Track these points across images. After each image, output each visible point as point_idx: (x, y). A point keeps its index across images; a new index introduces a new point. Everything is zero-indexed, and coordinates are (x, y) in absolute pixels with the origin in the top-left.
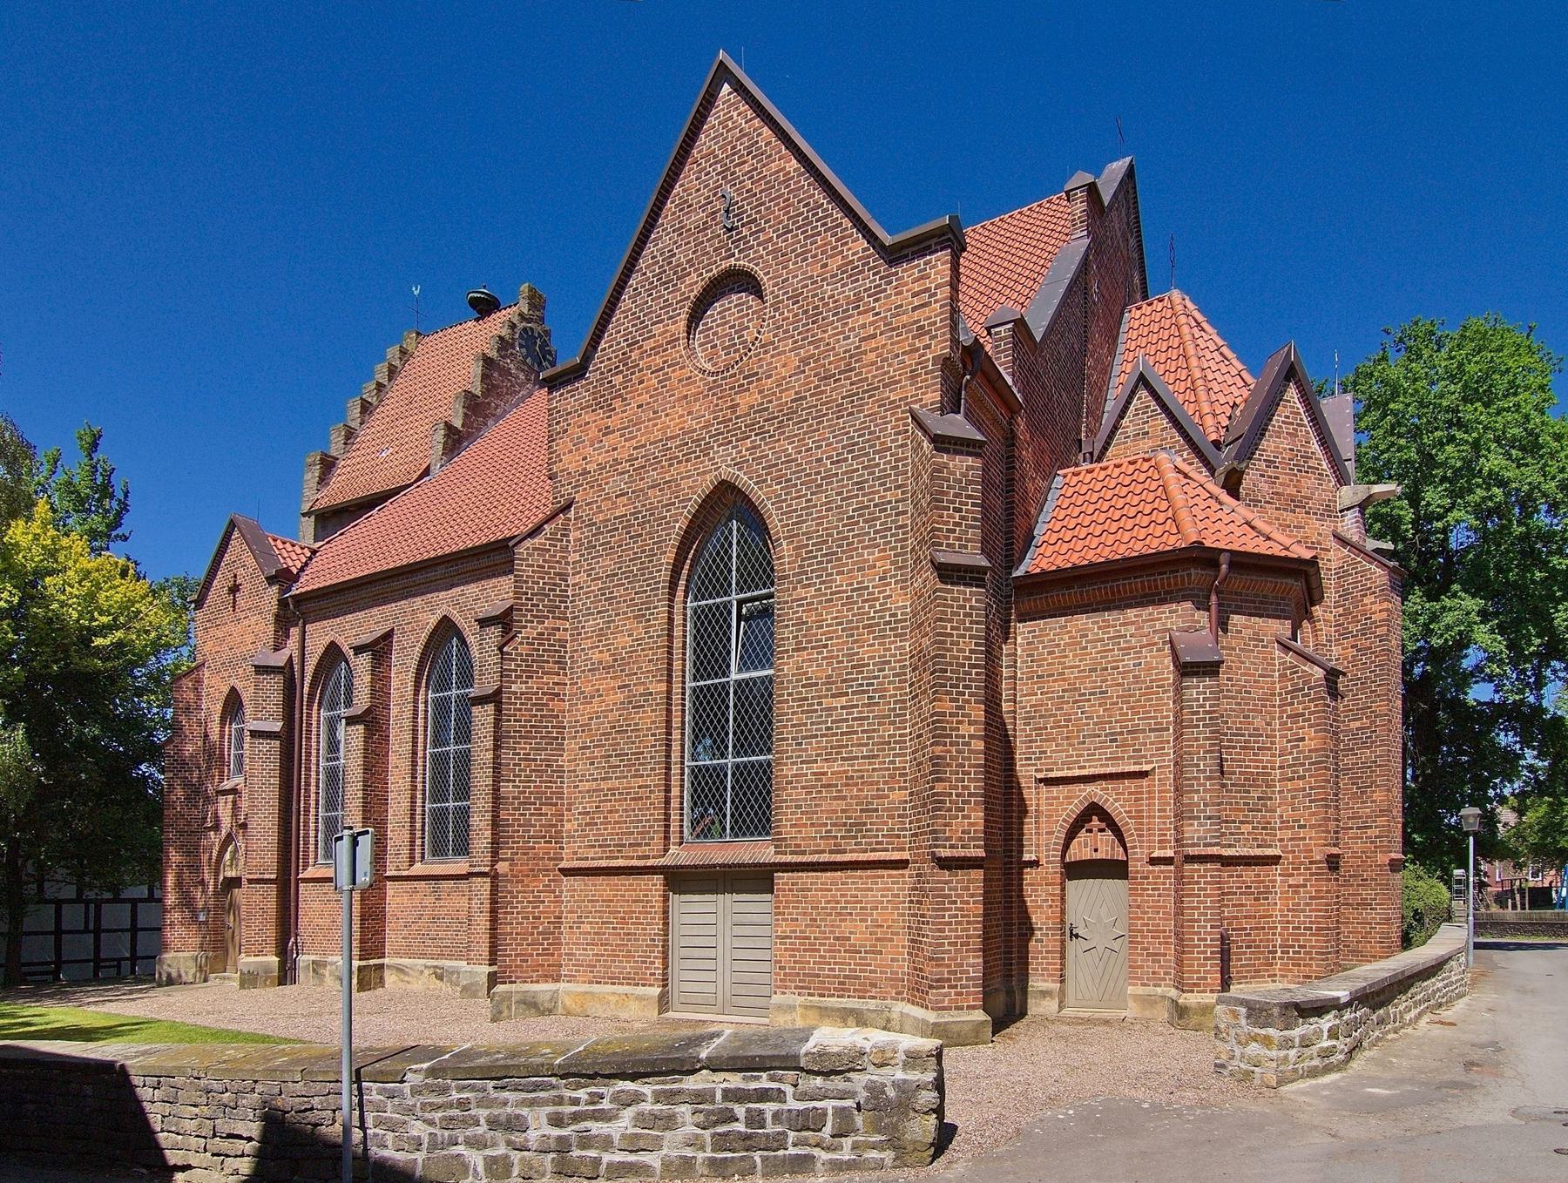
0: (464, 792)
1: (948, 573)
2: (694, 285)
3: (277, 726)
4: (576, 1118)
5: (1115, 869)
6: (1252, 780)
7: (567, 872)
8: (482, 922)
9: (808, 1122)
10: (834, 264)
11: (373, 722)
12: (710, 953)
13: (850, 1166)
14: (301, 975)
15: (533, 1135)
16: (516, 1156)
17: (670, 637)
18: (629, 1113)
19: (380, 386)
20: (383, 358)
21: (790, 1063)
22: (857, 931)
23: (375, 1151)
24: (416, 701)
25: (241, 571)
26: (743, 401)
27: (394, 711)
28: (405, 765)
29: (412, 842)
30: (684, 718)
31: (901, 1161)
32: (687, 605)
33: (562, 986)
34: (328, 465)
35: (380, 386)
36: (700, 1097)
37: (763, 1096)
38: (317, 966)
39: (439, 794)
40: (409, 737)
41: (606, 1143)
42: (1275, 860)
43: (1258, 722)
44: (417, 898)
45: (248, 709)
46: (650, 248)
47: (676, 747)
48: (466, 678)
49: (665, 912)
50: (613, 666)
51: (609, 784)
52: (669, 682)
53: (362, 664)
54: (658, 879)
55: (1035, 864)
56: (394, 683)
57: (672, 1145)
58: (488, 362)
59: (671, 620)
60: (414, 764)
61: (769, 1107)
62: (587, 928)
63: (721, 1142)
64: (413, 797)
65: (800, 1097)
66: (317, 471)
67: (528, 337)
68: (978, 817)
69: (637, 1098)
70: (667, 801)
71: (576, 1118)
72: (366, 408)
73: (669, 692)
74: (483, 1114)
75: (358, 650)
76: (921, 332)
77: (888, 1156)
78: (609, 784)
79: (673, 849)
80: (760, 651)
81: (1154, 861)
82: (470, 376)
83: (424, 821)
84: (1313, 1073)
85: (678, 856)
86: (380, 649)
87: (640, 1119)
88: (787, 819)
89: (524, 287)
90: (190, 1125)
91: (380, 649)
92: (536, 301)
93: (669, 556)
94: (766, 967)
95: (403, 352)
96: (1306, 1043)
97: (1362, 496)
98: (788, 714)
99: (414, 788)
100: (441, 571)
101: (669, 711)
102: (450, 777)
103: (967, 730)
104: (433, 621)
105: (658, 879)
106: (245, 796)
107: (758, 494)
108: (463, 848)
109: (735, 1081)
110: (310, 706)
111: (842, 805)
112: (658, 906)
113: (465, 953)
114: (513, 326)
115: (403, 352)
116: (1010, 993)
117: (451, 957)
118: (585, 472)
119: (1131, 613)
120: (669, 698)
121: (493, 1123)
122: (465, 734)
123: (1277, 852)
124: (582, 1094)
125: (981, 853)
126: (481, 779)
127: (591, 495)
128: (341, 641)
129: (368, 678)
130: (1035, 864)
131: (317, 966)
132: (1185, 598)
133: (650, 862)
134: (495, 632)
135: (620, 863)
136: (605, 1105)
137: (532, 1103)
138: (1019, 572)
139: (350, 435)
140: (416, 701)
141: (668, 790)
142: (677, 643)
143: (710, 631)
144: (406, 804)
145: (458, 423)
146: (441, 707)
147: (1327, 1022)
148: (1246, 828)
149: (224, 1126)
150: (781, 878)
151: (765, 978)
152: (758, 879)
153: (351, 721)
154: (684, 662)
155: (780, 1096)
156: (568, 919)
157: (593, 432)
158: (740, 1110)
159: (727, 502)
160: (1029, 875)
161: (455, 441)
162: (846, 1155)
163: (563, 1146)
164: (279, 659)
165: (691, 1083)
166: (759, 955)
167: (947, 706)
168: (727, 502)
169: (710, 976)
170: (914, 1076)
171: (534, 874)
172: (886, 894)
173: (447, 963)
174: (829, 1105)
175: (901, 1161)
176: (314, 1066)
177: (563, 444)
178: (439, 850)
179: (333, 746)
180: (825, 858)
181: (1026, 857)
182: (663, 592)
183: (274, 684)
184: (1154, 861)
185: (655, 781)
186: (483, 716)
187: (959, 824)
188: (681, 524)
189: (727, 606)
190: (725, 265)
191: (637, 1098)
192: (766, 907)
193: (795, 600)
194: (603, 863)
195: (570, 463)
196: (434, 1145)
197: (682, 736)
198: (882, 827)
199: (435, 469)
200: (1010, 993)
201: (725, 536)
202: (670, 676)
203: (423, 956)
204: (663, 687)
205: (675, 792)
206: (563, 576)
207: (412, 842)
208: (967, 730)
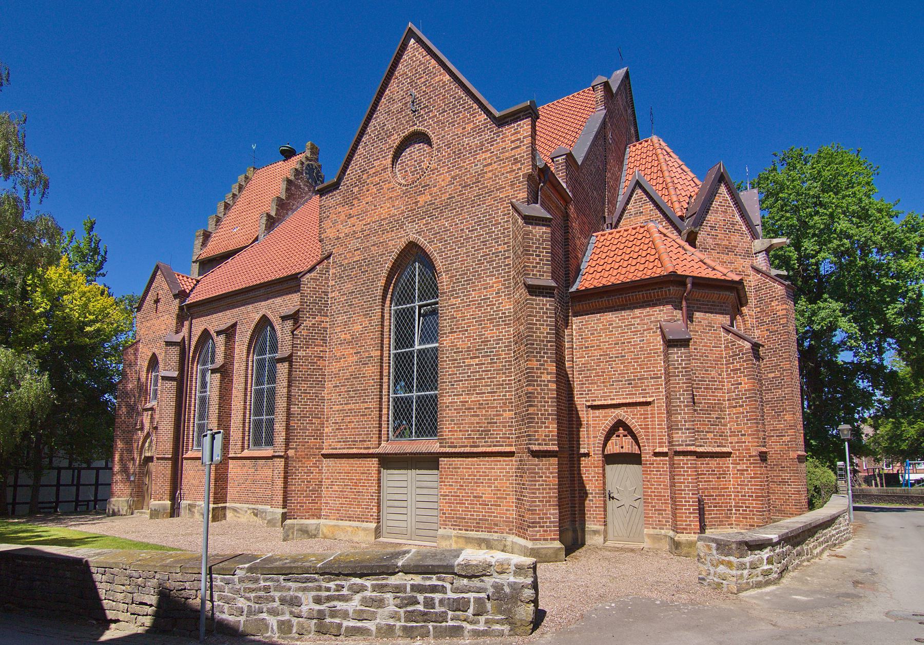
0: (271, 410)
2: (396, 139)
3: (175, 374)
4: (329, 599)
5: (634, 459)
6: (712, 408)
7: (326, 456)
8: (280, 483)
9: (460, 606)
10: (469, 128)
11: (225, 372)
13: (484, 633)
14: (182, 512)
15: (304, 608)
16: (295, 621)
18: (358, 597)
19: (234, 195)
21: (448, 570)
22: (486, 493)
23: (219, 616)
24: (247, 361)
26: (422, 199)
27: (236, 366)
30: (390, 370)
31: (513, 632)
33: (322, 521)
34: (207, 236)
35: (234, 195)
36: (398, 589)
37: (434, 589)
39: (258, 412)
40: (243, 380)
41: (345, 615)
42: (728, 455)
44: (245, 469)
45: (161, 365)
46: (373, 122)
47: (385, 386)
48: (274, 349)
50: (352, 342)
51: (349, 407)
52: (382, 350)
53: (220, 340)
54: (375, 461)
55: (587, 455)
56: (237, 351)
57: (382, 617)
58: (289, 182)
59: (383, 316)
60: (246, 395)
61: (437, 596)
62: (336, 488)
63: (410, 616)
64: (245, 413)
66: (201, 239)
67: (310, 169)
68: (553, 427)
69: (363, 588)
70: (380, 417)
71: (329, 599)
72: (227, 207)
73: (382, 356)
74: (277, 595)
75: (219, 333)
76: (516, 161)
77: (506, 628)
78: (349, 407)
79: (383, 444)
81: (656, 454)
82: (279, 189)
84: (759, 585)
85: (386, 447)
86: (229, 333)
87: (364, 601)
88: (446, 427)
89: (309, 144)
90: (120, 596)
91: (229, 333)
92: (314, 151)
94: (435, 513)
95: (247, 178)
96: (753, 566)
99: (245, 408)
101: (381, 367)
102: (263, 402)
104: (257, 317)
105: (375, 461)
107: (430, 248)
108: (270, 442)
109: (418, 580)
111: (477, 419)
112: (375, 476)
113: (269, 501)
114: (302, 163)
115: (247, 178)
117: (262, 503)
118: (338, 238)
121: (283, 601)
122: (273, 379)
123: (729, 450)
124: (332, 585)
125: (556, 448)
127: (341, 250)
129: (223, 348)
130: (587, 455)
132: (667, 303)
133: (371, 451)
134: (290, 323)
135: (355, 451)
136: (345, 592)
137: (304, 589)
139: (218, 220)
140: (247, 361)
141: (381, 411)
142: (386, 329)
143: (404, 322)
144: (240, 417)
145: (273, 214)
147: (766, 553)
148: (710, 436)
149: (138, 598)
150: (443, 461)
151: (435, 519)
152: (429, 461)
153: (214, 371)
154: (390, 339)
155: (443, 590)
156: (326, 482)
157: (343, 217)
158: (420, 597)
159: (414, 253)
160: (584, 461)
161: (272, 223)
162: (481, 627)
163: (321, 616)
164: (178, 338)
165: (393, 580)
168: (414, 253)
170: (520, 580)
171: (307, 456)
173: (260, 507)
174: (471, 596)
175: (513, 632)
176: (187, 565)
177: (327, 224)
178: (257, 443)
179: (204, 385)
181: (582, 451)
182: (378, 302)
183: (175, 351)
184: (656, 454)
185: (374, 405)
187: (543, 431)
188: (388, 265)
189: (413, 309)
190: (412, 129)
191: (363, 588)
192: (434, 478)
193: (452, 306)
194: (345, 451)
195: (330, 233)
196: (250, 613)
198: (499, 433)
199: (261, 238)
201: (412, 275)
203: (247, 502)
204: (378, 353)
205: (385, 411)
206: (326, 293)
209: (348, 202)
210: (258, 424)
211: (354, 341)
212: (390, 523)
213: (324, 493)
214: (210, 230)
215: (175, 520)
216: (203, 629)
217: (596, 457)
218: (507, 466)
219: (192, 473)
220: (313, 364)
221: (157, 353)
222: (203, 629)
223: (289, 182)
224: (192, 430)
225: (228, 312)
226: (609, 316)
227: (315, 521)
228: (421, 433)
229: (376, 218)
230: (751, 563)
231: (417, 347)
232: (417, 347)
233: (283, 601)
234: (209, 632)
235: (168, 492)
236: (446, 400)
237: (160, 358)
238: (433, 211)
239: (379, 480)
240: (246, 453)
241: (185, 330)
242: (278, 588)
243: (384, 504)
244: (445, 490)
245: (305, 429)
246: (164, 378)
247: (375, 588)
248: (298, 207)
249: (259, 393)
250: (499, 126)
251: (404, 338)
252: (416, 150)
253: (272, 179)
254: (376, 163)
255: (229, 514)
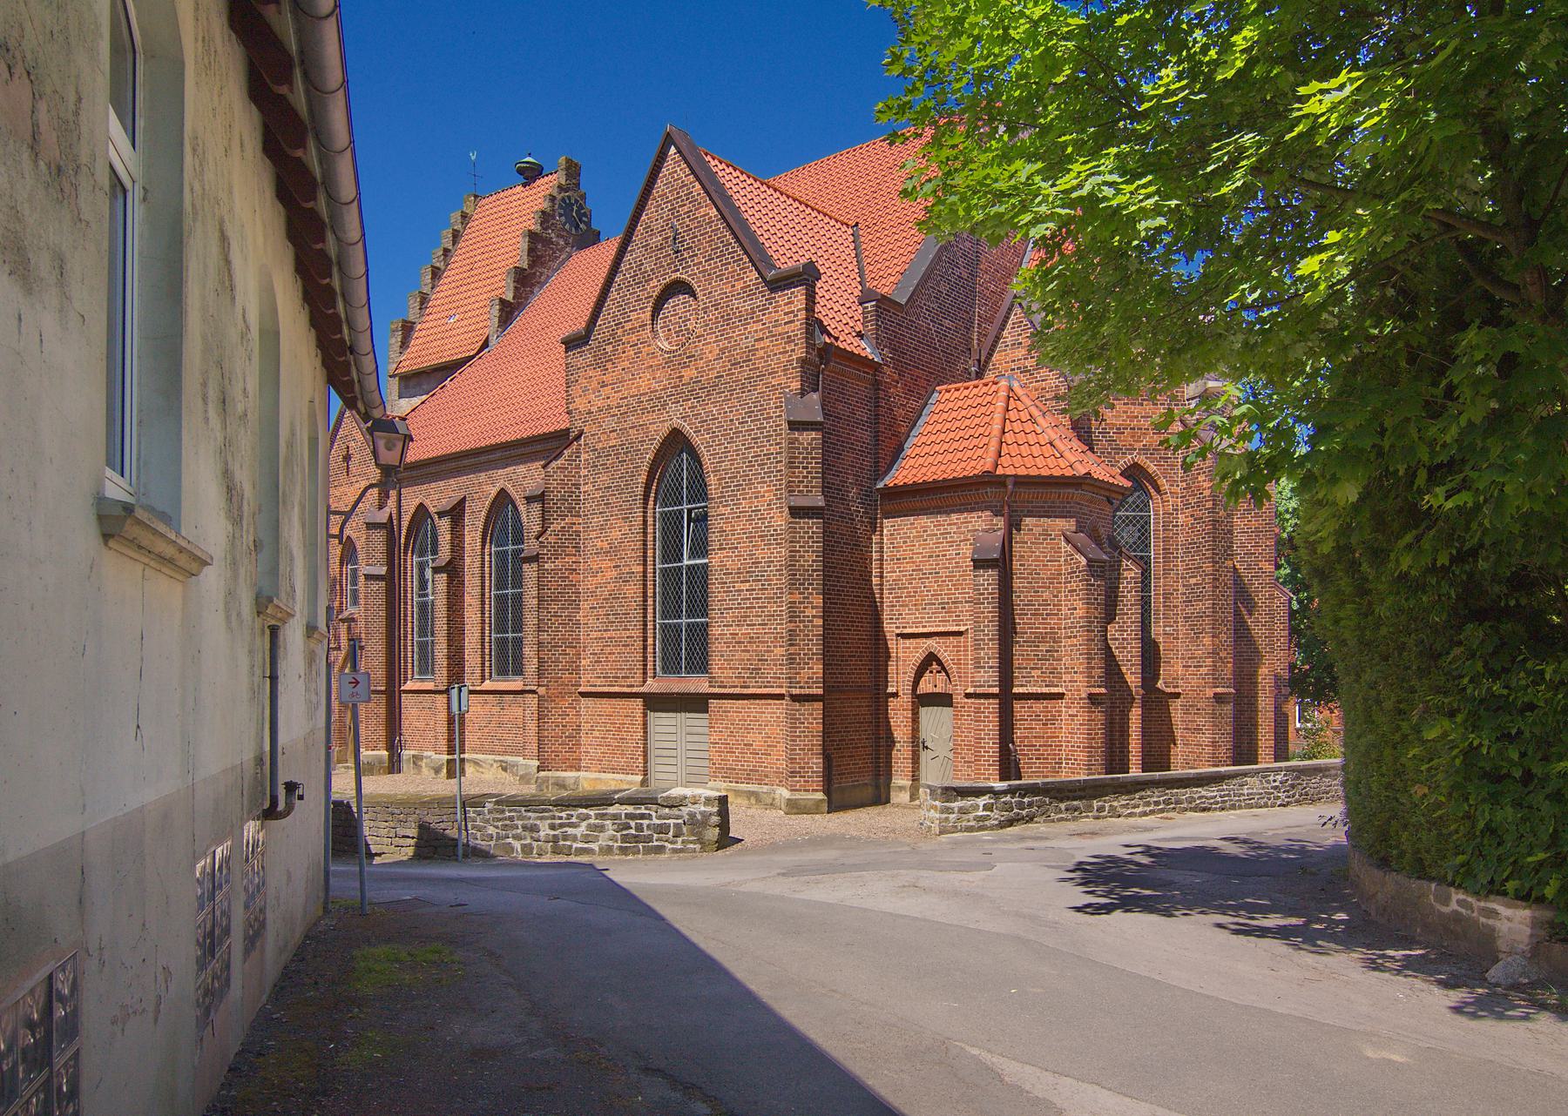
0: (519, 627)
1: (796, 512)
2: (655, 287)
3: (383, 570)
4: (561, 826)
5: (944, 700)
6: (1042, 638)
7: (583, 695)
8: (532, 726)
9: (663, 829)
10: (739, 285)
11: (453, 570)
12: (673, 753)
13: (681, 851)
14: (404, 766)
15: (542, 834)
16: (535, 844)
17: (645, 533)
18: (584, 824)
19: (446, 251)
20: (447, 224)
21: (654, 801)
22: (756, 739)
23: (472, 842)
24: (483, 554)
25: (352, 444)
26: (688, 374)
27: (468, 561)
28: (476, 603)
29: (483, 664)
30: (655, 587)
31: (703, 849)
32: (656, 510)
33: (581, 774)
34: (408, 329)
35: (446, 251)
36: (615, 817)
37: (642, 817)
38: (416, 759)
39: (501, 628)
40: (478, 582)
41: (575, 838)
42: (1061, 696)
43: (1046, 595)
44: (488, 707)
45: (361, 556)
46: (628, 257)
47: (650, 610)
48: (519, 539)
49: (645, 724)
50: (609, 551)
51: (609, 634)
52: (645, 564)
53: (444, 525)
54: (639, 701)
55: (895, 695)
56: (467, 539)
57: (603, 840)
58: (532, 236)
59: (645, 522)
60: (483, 603)
61: (645, 822)
62: (596, 734)
63: (625, 839)
64: (483, 629)
65: (659, 818)
66: (399, 336)
67: (567, 206)
68: (818, 668)
69: (588, 817)
70: (645, 648)
71: (561, 826)
72: (436, 274)
73: (645, 572)
74: (520, 823)
75: (441, 514)
76: (790, 340)
77: (698, 847)
78: (609, 634)
79: (650, 681)
80: (701, 547)
81: (968, 696)
82: (515, 253)
83: (491, 648)
84: (970, 829)
85: (652, 686)
86: (456, 513)
87: (589, 827)
88: (716, 663)
89: (562, 160)
90: (383, 832)
91: (456, 513)
92: (573, 170)
93: (642, 478)
94: (706, 763)
95: (464, 216)
96: (963, 811)
97: (1200, 390)
98: (717, 593)
99: (483, 622)
100: (498, 454)
101: (645, 585)
102: (507, 614)
103: (810, 612)
104: (494, 492)
105: (639, 701)
106: (361, 624)
107: (696, 440)
108: (519, 671)
109: (630, 809)
110: (406, 553)
111: (746, 656)
112: (640, 720)
113: (520, 751)
114: (553, 199)
115: (464, 216)
116: (877, 787)
117: (512, 753)
118: (590, 412)
119: (954, 516)
120: (645, 576)
121: (525, 828)
122: (518, 582)
123: (1060, 690)
124: (563, 814)
125: (820, 691)
126: (530, 620)
127: (594, 430)
128: (427, 503)
129: (448, 537)
130: (895, 695)
131: (416, 759)
132: (986, 508)
133: (634, 690)
134: (537, 506)
135: (616, 689)
136: (574, 820)
137: (541, 818)
138: (888, 481)
139: (424, 300)
140: (483, 554)
141: (645, 640)
142: (650, 537)
143: (671, 526)
144: (477, 635)
145: (509, 297)
146: (501, 556)
147: (982, 801)
148: (1035, 673)
149: (401, 832)
150: (713, 703)
151: (706, 771)
152: (696, 703)
153: (436, 570)
154: (655, 550)
155: (649, 817)
156: (585, 727)
157: (594, 384)
158: (633, 824)
159: (676, 443)
160: (892, 703)
161: (508, 312)
162: (679, 846)
163: (555, 839)
164: (382, 517)
165: (611, 810)
166: (702, 755)
167: (798, 597)
168: (676, 443)
169: (673, 769)
170: (709, 809)
171: (562, 695)
172: (776, 712)
173: (509, 758)
174: (671, 821)
175: (703, 849)
176: (442, 802)
177: (575, 390)
178: (503, 672)
179: (423, 584)
180: (737, 691)
181: (890, 690)
182: (639, 503)
183: (379, 537)
184: (968, 696)
185: (637, 633)
186: (529, 571)
187: (806, 673)
188: (650, 456)
189: (681, 512)
190: (674, 276)
191: (588, 817)
192: (706, 723)
193: (722, 516)
194: (606, 689)
195: (580, 404)
196: (498, 838)
197: (655, 605)
198: (770, 672)
199: (493, 341)
200: (877, 787)
201: (676, 471)
202: (645, 561)
203: (492, 752)
204: (640, 568)
205: (650, 641)
206: (577, 486)
207: (483, 664)
208: (810, 612)
209: (602, 362)
210: (502, 643)
211: (612, 551)
212: (659, 776)
213: (583, 740)
214: (411, 318)
215: (396, 776)
216: (460, 852)
217: (905, 699)
218: (778, 710)
219: (414, 711)
220: (564, 578)
221: (353, 536)
222: (460, 852)
223: (532, 236)
224: (411, 654)
225: (452, 481)
226: (924, 520)
227: (574, 774)
228: (691, 669)
229: (634, 391)
230: (960, 808)
231: (686, 562)
232: (686, 562)
233: (525, 828)
234: (465, 856)
235: (383, 739)
236: (715, 631)
237: (358, 546)
238: (698, 391)
239: (645, 724)
240: (488, 685)
241: (392, 503)
242: (521, 818)
243: (652, 753)
244: (715, 738)
245: (557, 661)
246: (368, 577)
247: (598, 816)
248: (549, 277)
249: (501, 600)
250: (773, 290)
251: (672, 551)
252: (677, 303)
253: (511, 214)
254: (633, 316)
255: (469, 769)
